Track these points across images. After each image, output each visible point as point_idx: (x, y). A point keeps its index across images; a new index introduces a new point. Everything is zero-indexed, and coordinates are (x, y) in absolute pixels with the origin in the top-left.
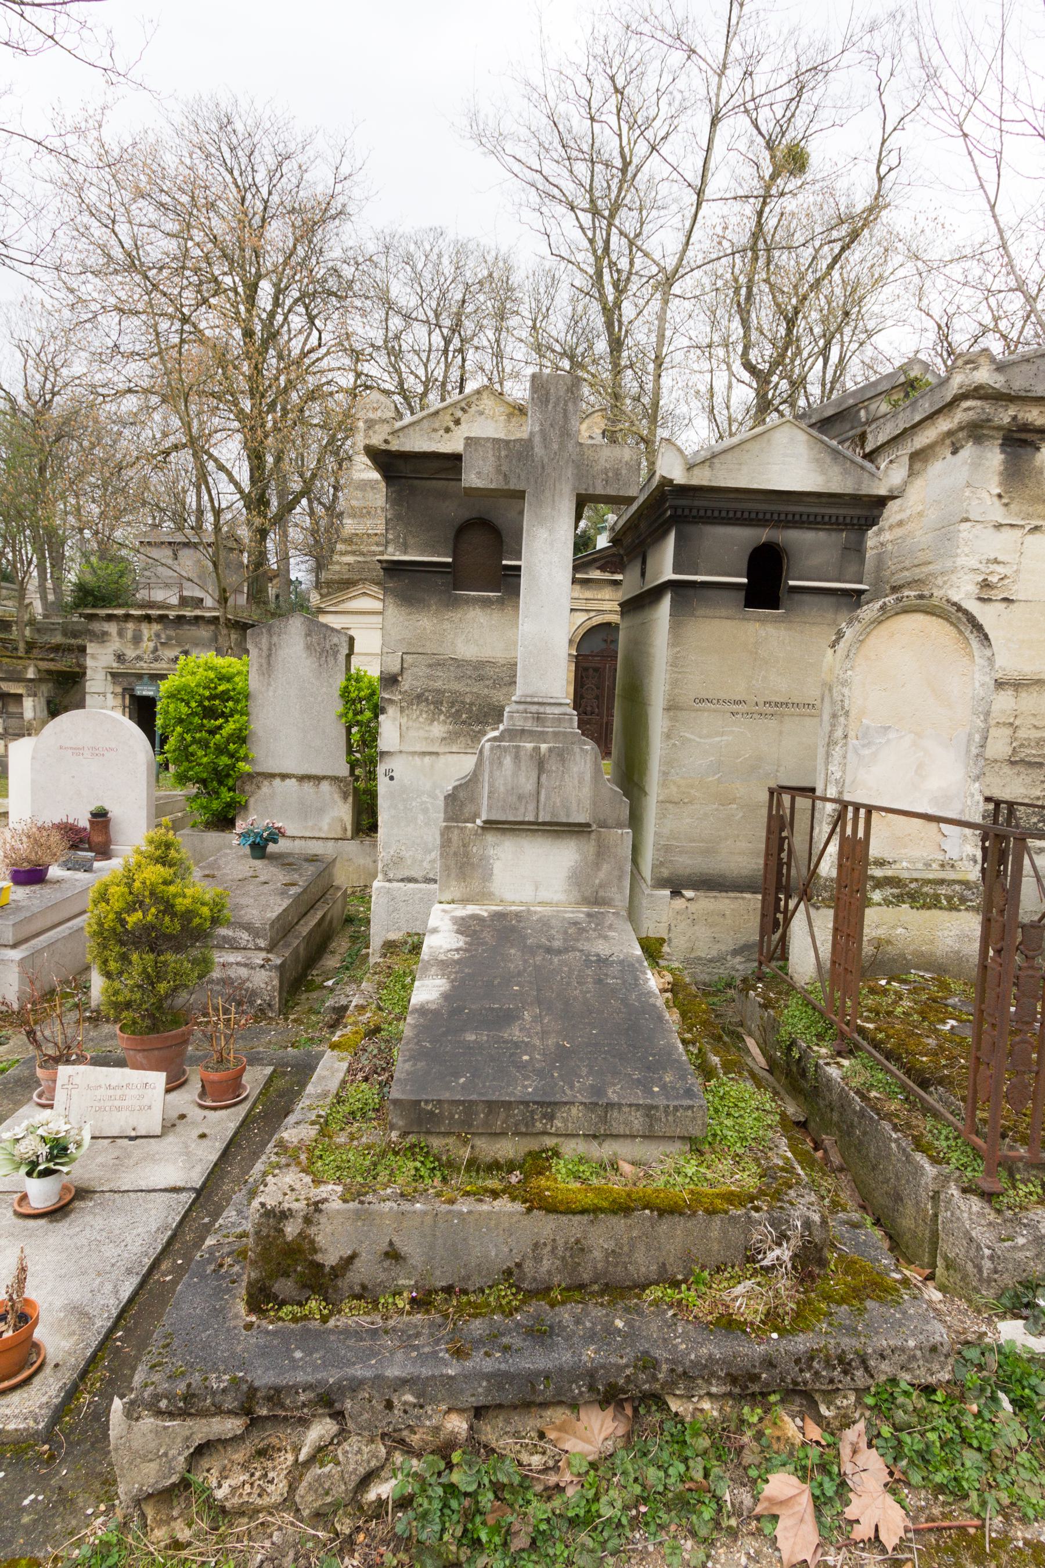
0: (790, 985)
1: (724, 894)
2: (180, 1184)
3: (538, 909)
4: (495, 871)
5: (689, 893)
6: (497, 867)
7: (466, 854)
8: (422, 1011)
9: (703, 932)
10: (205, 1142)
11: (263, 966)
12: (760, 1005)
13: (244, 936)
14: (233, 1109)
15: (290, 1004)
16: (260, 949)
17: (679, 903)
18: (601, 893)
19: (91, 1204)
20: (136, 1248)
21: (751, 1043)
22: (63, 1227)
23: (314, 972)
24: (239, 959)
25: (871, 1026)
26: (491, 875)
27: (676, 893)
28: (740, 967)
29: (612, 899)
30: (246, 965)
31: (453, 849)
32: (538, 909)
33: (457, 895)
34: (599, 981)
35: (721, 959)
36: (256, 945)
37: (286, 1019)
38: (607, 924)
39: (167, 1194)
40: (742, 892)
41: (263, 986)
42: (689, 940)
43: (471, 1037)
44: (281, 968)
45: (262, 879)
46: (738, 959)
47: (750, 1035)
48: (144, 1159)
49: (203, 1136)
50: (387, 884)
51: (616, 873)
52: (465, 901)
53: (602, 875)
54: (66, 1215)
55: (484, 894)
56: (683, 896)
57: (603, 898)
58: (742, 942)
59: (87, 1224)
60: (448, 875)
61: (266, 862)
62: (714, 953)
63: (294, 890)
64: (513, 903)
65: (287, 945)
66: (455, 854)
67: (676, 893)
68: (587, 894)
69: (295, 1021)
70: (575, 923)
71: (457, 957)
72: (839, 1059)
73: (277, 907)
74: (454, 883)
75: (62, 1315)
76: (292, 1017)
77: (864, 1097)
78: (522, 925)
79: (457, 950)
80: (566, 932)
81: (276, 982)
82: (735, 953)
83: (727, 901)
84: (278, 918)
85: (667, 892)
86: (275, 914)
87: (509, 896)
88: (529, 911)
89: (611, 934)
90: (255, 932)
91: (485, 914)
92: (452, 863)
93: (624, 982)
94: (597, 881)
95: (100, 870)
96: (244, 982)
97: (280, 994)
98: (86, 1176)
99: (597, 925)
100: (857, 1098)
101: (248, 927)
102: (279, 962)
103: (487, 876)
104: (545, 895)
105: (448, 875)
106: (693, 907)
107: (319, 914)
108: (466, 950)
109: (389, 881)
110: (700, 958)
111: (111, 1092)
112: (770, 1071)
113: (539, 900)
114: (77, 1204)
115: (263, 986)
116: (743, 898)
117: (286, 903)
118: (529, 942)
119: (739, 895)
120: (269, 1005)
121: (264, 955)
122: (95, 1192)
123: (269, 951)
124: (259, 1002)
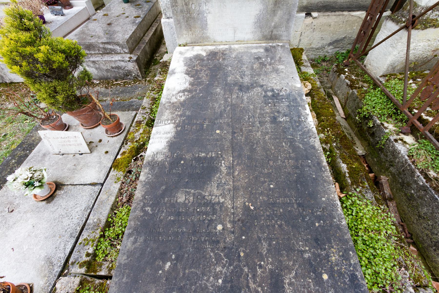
0: (363, 70)
1: (333, 13)
2: (96, 181)
3: (236, 46)
4: (209, 22)
5: (315, 14)
6: (210, 19)
7: (189, 11)
8: (152, 164)
9: (317, 35)
10: (108, 155)
11: (129, 61)
12: (347, 85)
13: (118, 48)
14: (119, 136)
15: (147, 73)
16: (126, 53)
17: (309, 19)
18: (275, 32)
19: (62, 192)
20: (76, 221)
21: (336, 99)
22: (52, 206)
23: (157, 55)
24: (120, 58)
25: (430, 119)
26: (206, 25)
27: (308, 14)
28: (329, 51)
29: (281, 36)
30: (123, 61)
31: (180, 8)
32: (236, 46)
33: (188, 40)
34: (274, 120)
35: (323, 47)
36: (124, 51)
37: (146, 80)
38: (277, 58)
39: (90, 186)
40: (343, 11)
41: (133, 69)
42: (310, 40)
43: (181, 198)
44: (137, 61)
45: (126, 15)
46: (331, 47)
47: (336, 95)
48: (84, 166)
49: (107, 152)
50: (167, 20)
51: (286, 17)
52: (193, 43)
53: (276, 19)
54: (53, 199)
55: (203, 38)
56: (311, 16)
57: (276, 36)
58: (335, 39)
59: (62, 201)
60: (181, 27)
61: (129, 4)
62: (320, 45)
63: (139, 20)
64: (221, 43)
65: (139, 49)
66: (182, 11)
67: (308, 14)
68: (266, 33)
69: (149, 81)
70: (258, 58)
71: (183, 98)
72: (402, 136)
73: (130, 29)
74: (185, 32)
75: (43, 263)
76: (148, 79)
77: (426, 177)
78: (226, 62)
79: (184, 91)
80: (252, 68)
81: (137, 67)
82: (330, 44)
83: (334, 17)
84: (131, 37)
85: (303, 14)
86: (129, 36)
87: (219, 38)
88: (230, 49)
89: (281, 67)
90: (122, 47)
91: (204, 54)
92: (181, 18)
93: (291, 119)
94: (273, 24)
95: (68, 14)
96: (125, 67)
97: (140, 70)
98: (63, 176)
99: (272, 59)
100: (422, 177)
101: (118, 44)
102: (135, 58)
103: (204, 27)
104: (240, 36)
105: (181, 27)
106: (315, 22)
107: (154, 29)
108: (190, 91)
109: (168, 18)
110: (313, 48)
111: (64, 140)
112: (346, 119)
113: (237, 39)
114: (58, 192)
115: (133, 69)
116: (343, 15)
117: (135, 27)
118: (229, 78)
119: (341, 13)
120: (138, 76)
121: (129, 55)
122: (65, 185)
123: (131, 54)
124: (134, 75)
